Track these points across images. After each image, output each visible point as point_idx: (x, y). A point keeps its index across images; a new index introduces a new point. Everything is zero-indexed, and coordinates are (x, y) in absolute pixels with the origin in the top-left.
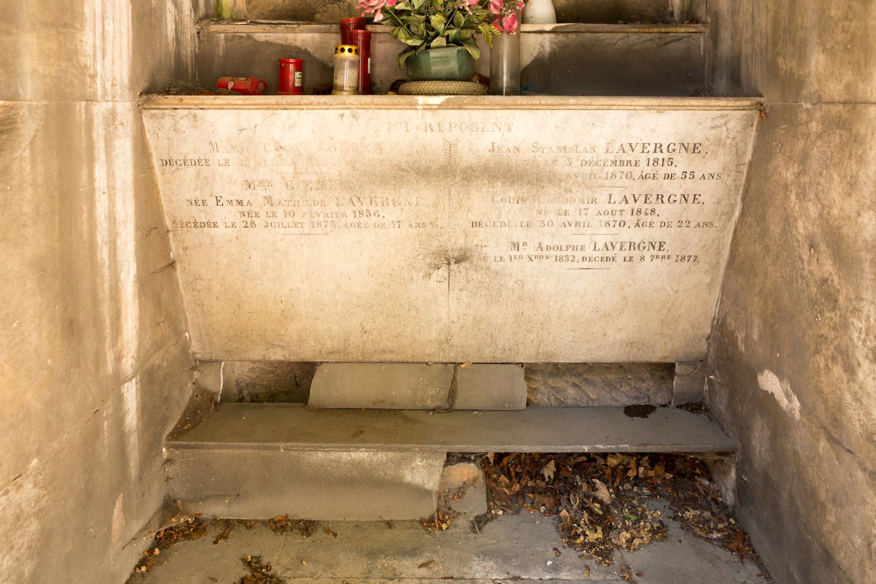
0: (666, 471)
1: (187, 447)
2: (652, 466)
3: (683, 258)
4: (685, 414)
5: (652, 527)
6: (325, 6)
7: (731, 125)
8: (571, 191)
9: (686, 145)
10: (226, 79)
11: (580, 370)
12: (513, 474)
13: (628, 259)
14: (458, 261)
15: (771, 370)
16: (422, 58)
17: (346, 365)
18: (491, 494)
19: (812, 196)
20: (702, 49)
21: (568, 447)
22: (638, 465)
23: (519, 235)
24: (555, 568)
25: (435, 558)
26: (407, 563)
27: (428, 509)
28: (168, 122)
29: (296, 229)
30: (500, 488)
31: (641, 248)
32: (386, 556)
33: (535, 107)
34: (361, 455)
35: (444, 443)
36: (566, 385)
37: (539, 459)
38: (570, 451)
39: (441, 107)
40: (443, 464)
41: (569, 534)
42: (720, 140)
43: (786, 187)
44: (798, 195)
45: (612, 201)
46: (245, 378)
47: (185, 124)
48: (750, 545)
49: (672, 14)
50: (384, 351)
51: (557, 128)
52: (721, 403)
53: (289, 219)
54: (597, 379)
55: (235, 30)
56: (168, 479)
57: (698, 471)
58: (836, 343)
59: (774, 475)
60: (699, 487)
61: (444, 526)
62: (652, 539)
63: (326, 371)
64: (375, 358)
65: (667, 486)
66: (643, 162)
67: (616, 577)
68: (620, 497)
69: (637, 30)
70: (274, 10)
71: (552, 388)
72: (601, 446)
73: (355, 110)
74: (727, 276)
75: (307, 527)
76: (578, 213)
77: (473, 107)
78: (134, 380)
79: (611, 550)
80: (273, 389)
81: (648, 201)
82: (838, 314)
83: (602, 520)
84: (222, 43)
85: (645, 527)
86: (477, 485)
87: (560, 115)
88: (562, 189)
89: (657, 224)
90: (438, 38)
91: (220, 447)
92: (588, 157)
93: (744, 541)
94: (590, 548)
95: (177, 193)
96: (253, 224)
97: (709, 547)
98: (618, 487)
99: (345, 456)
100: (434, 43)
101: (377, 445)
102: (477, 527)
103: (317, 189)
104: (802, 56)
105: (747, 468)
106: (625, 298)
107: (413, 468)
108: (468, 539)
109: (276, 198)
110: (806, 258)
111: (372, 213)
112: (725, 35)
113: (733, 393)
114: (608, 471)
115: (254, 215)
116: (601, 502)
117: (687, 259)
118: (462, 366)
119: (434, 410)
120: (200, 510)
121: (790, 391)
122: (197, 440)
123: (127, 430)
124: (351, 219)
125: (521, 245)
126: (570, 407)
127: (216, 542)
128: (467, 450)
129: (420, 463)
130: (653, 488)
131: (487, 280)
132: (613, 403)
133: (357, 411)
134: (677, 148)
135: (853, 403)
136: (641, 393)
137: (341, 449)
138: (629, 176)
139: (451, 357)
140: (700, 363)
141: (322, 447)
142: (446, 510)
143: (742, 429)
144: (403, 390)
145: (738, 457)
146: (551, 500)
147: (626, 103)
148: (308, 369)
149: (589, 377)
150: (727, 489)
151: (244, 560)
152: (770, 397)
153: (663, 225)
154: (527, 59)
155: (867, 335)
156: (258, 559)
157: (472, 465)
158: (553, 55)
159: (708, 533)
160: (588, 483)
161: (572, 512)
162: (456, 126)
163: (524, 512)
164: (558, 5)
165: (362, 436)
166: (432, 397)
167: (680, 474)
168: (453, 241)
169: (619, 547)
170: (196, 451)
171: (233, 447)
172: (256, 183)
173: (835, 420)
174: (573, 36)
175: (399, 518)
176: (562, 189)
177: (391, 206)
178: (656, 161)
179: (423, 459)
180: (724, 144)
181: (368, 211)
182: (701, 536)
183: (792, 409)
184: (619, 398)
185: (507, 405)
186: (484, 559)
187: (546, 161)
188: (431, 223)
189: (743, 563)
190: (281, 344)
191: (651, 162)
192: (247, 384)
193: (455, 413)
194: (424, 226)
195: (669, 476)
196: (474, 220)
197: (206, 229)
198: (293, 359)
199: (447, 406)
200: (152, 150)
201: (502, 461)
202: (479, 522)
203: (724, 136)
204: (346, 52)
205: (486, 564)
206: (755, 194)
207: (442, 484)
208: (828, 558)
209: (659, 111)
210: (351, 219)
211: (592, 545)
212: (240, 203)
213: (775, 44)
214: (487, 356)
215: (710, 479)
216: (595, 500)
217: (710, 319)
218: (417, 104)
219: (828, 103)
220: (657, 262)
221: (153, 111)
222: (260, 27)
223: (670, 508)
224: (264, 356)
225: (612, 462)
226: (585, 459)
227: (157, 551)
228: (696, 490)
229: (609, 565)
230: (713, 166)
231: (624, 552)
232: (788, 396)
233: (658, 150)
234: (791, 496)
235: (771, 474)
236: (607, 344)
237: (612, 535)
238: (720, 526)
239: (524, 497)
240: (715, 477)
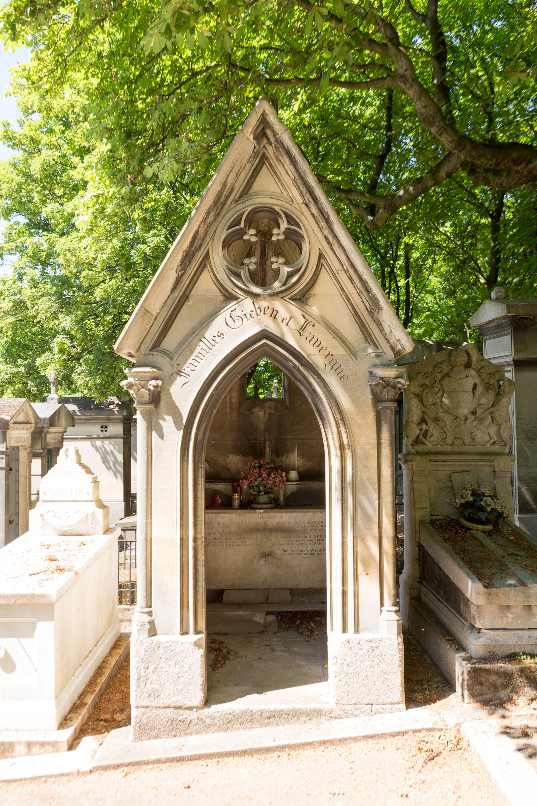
14: (268, 555)
18: (279, 626)
23: (285, 547)
34: (241, 613)
99: (237, 613)
124: (237, 543)
138: (315, 530)
139: (267, 586)
144: (252, 597)
154: (288, 493)
158: (297, 491)
198: (218, 588)
210: (237, 543)
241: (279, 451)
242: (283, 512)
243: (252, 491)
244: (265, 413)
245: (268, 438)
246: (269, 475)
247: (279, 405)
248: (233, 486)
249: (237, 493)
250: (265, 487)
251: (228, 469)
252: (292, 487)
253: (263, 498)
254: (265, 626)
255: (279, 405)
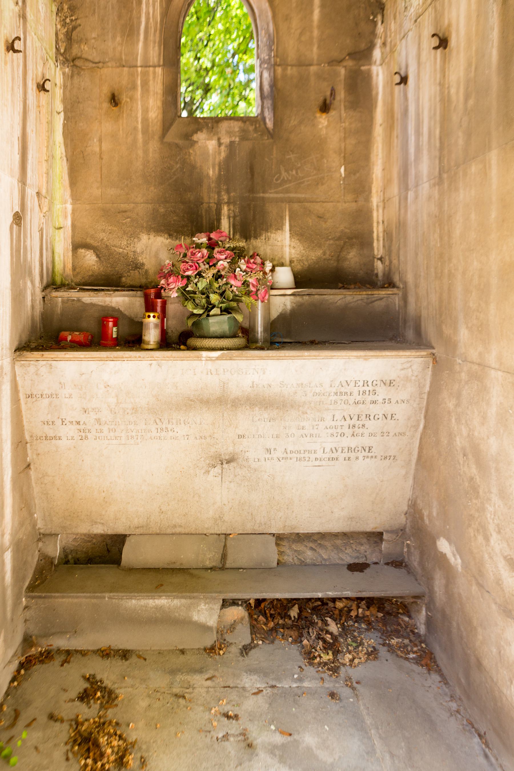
0: (378, 611)
1: (40, 597)
2: (368, 608)
3: (386, 458)
4: (391, 569)
5: (367, 651)
6: (129, 272)
7: (414, 367)
8: (307, 413)
9: (385, 381)
10: (64, 333)
11: (315, 538)
12: (269, 615)
13: (347, 459)
14: (228, 462)
15: (444, 537)
16: (204, 322)
17: (147, 537)
18: (254, 629)
19: (464, 422)
20: (397, 306)
21: (307, 594)
22: (358, 607)
24: (300, 680)
25: (216, 674)
26: (198, 678)
27: (209, 641)
28: (32, 369)
29: (116, 441)
30: (259, 625)
31: (356, 451)
32: (182, 673)
33: (281, 358)
34: (162, 602)
35: (220, 592)
36: (305, 548)
37: (287, 604)
38: (309, 597)
39: (218, 358)
40: (219, 607)
41: (309, 656)
42: (407, 377)
43: (449, 412)
44: (456, 419)
45: (335, 419)
46: (70, 546)
47: (43, 370)
48: (435, 662)
49: (377, 275)
50: (175, 526)
51: (296, 371)
52: (415, 561)
53: (112, 434)
54: (327, 544)
55: (69, 296)
56: (26, 621)
57: (401, 611)
58: (479, 520)
59: (448, 611)
60: (401, 622)
61: (221, 652)
62: (368, 659)
63: (133, 541)
64: (169, 531)
65: (379, 622)
66: (356, 393)
67: (342, 685)
68: (345, 630)
69: (351, 293)
70: (92, 275)
71: (296, 551)
72: (330, 593)
73: (160, 361)
74: (416, 470)
75: (125, 655)
76: (311, 428)
77: (240, 358)
78: (10, 550)
79: (339, 667)
80: (90, 554)
81: (360, 419)
82: (480, 501)
83: (334, 647)
84: (60, 304)
85: (362, 651)
86: (244, 622)
87: (299, 363)
88: (300, 412)
89: (366, 434)
90: (215, 309)
91: (63, 597)
92: (318, 390)
93: (431, 659)
94: (324, 666)
95: (35, 417)
96: (86, 437)
97: (407, 664)
98: (343, 623)
100: (212, 312)
101: (174, 594)
102: (244, 653)
103: (132, 414)
104: (456, 330)
105: (432, 607)
106: (346, 486)
107: (199, 611)
108: (238, 661)
109: (103, 419)
110: (461, 462)
111: (169, 430)
112: (411, 299)
113: (422, 554)
114: (337, 612)
115: (87, 431)
116: (331, 634)
117: (388, 458)
118: (231, 536)
119: (211, 569)
120: (50, 642)
121: (455, 552)
122: (47, 592)
123: (6, 585)
125: (272, 451)
126: (309, 565)
127: (62, 665)
128: (237, 597)
129: (203, 607)
130: (369, 623)
131: (249, 475)
132: (340, 562)
133: (156, 570)
134: (379, 383)
135: (489, 560)
136: (360, 554)
137: (148, 597)
138: (346, 402)
139: (223, 529)
140: (400, 532)
141: (135, 596)
142: (222, 641)
143: (428, 579)
144: (189, 555)
145: (426, 599)
146: (296, 633)
147: (343, 355)
148: (120, 540)
149: (322, 543)
150: (420, 623)
151: (84, 677)
152: (444, 556)
153: (371, 435)
154: (275, 314)
155: (495, 515)
156: (94, 676)
157: (240, 608)
159: (406, 654)
160: (322, 620)
161: (311, 641)
162: (228, 371)
163: (277, 642)
164: (296, 269)
165: (162, 588)
166: (210, 559)
167: (389, 613)
168: (225, 448)
169: (344, 665)
170: (46, 600)
171: (73, 597)
172: (90, 410)
173: (480, 571)
174: (307, 298)
175: (189, 647)
176: (300, 412)
177: (183, 425)
178: (364, 392)
179: (205, 604)
180: (411, 380)
181: (167, 428)
182: (401, 657)
183: (457, 565)
184: (344, 558)
185: (263, 564)
186: (250, 675)
187: (289, 394)
188: (210, 436)
189: (429, 674)
190: (102, 521)
191: (361, 393)
192: (72, 551)
193: (226, 570)
194: (205, 438)
195: (380, 615)
196: (240, 434)
197: (53, 441)
198: (110, 532)
199: (221, 566)
200: (20, 388)
201: (260, 605)
202: (245, 649)
203: (410, 375)
204: (152, 317)
205: (252, 677)
206: (432, 416)
207: (219, 622)
208: (479, 664)
209: (366, 359)
211: (326, 664)
212: (78, 423)
213: (441, 316)
214: (249, 528)
215: (410, 617)
216: (327, 632)
217: (407, 500)
218: (202, 357)
219: (470, 362)
220: (368, 460)
221: (23, 362)
222: (87, 293)
223: (381, 638)
224: (89, 530)
225: (340, 605)
226: (320, 603)
227: (23, 672)
228: (399, 624)
229: (337, 677)
230: (404, 395)
231: (348, 668)
232: (454, 555)
233: (366, 385)
234: (458, 624)
235: (446, 610)
236: (335, 521)
237: (339, 656)
238: (415, 649)
239: (276, 632)
240: (413, 615)
241: (251, 224)
242: (268, 358)
243: (190, 307)
244: (220, 144)
245: (225, 197)
246: (233, 263)
247: (251, 128)
248: (146, 297)
249: (154, 310)
250: (222, 294)
251: (137, 266)
252: (282, 302)
253: (217, 323)
254: (220, 632)
255: (251, 128)
